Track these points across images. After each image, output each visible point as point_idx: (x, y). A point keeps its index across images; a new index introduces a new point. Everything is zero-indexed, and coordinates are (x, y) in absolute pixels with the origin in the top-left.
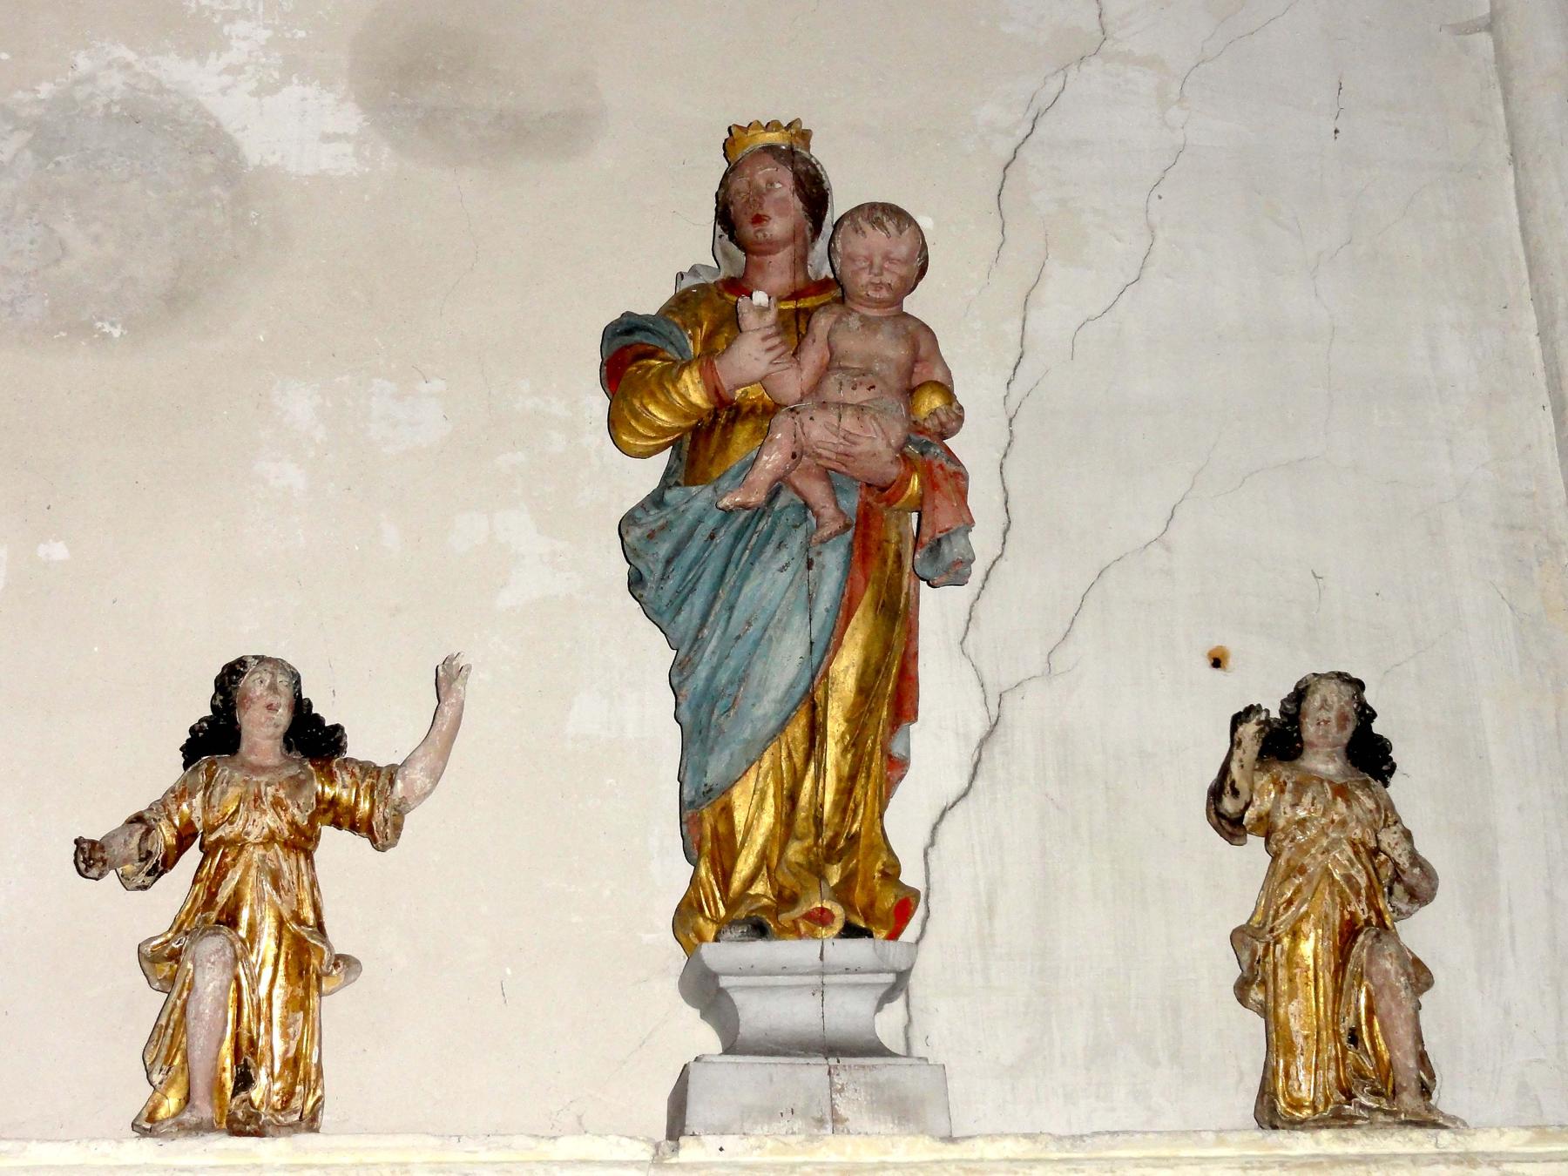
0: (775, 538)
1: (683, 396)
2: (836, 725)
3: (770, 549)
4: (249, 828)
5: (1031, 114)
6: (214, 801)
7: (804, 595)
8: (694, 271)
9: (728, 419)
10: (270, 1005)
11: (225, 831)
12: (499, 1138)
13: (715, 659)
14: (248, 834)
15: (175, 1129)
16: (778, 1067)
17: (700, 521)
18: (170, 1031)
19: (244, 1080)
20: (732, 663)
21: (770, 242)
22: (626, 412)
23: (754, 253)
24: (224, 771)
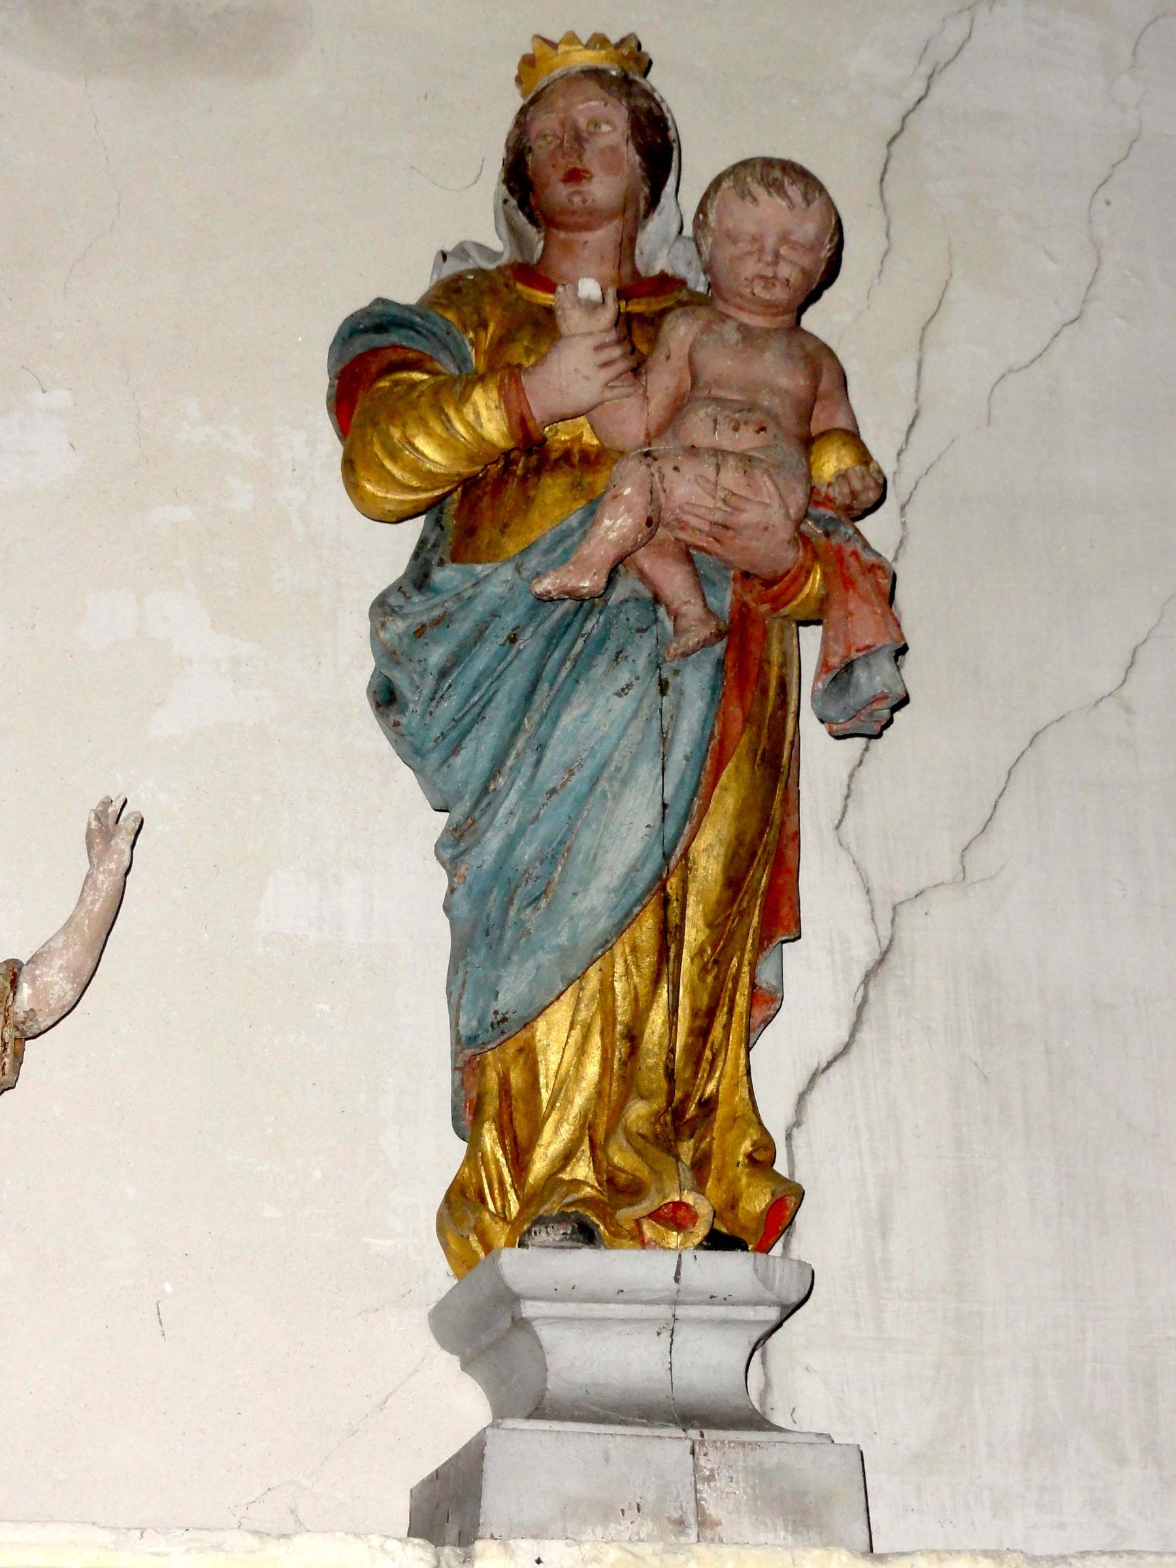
0: (611, 646)
1: (467, 424)
2: (694, 934)
3: (602, 662)
5: (925, 70)
7: (655, 736)
8: (462, 251)
9: (527, 470)
12: (204, 1534)
13: (514, 824)
16: (618, 1440)
17: (495, 614)
20: (543, 830)
21: (591, 212)
22: (377, 449)
23: (558, 226)
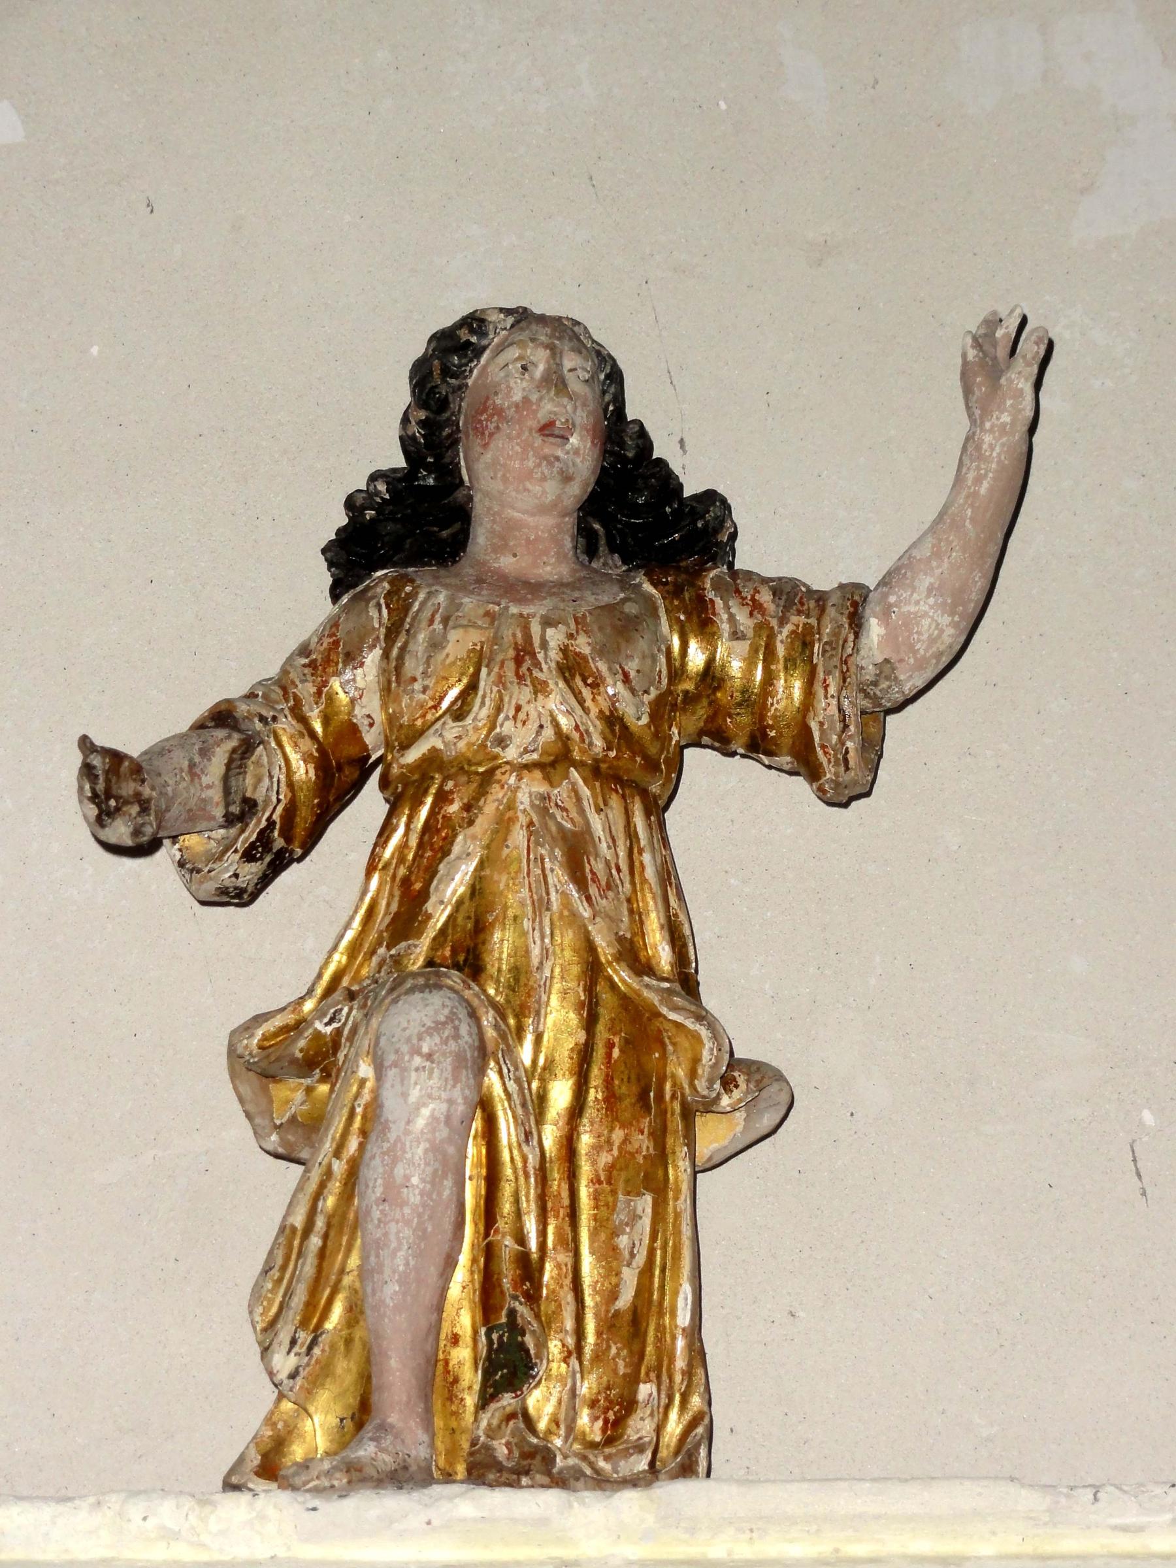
4: (507, 728)
6: (412, 666)
10: (572, 1176)
11: (446, 738)
14: (502, 742)
15: (340, 1480)
18: (315, 1241)
19: (509, 1367)
24: (431, 594)
